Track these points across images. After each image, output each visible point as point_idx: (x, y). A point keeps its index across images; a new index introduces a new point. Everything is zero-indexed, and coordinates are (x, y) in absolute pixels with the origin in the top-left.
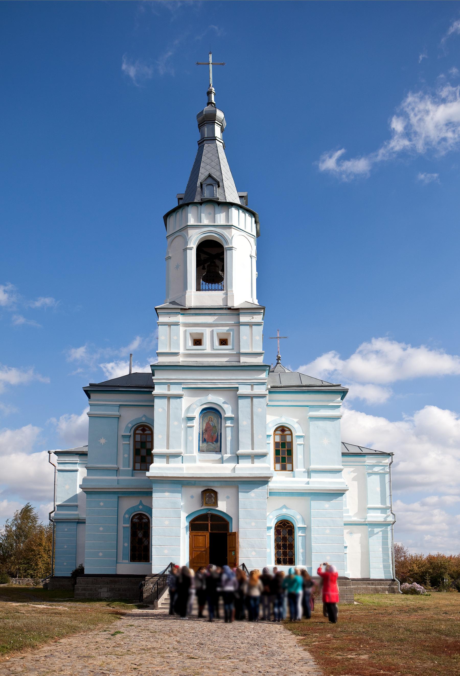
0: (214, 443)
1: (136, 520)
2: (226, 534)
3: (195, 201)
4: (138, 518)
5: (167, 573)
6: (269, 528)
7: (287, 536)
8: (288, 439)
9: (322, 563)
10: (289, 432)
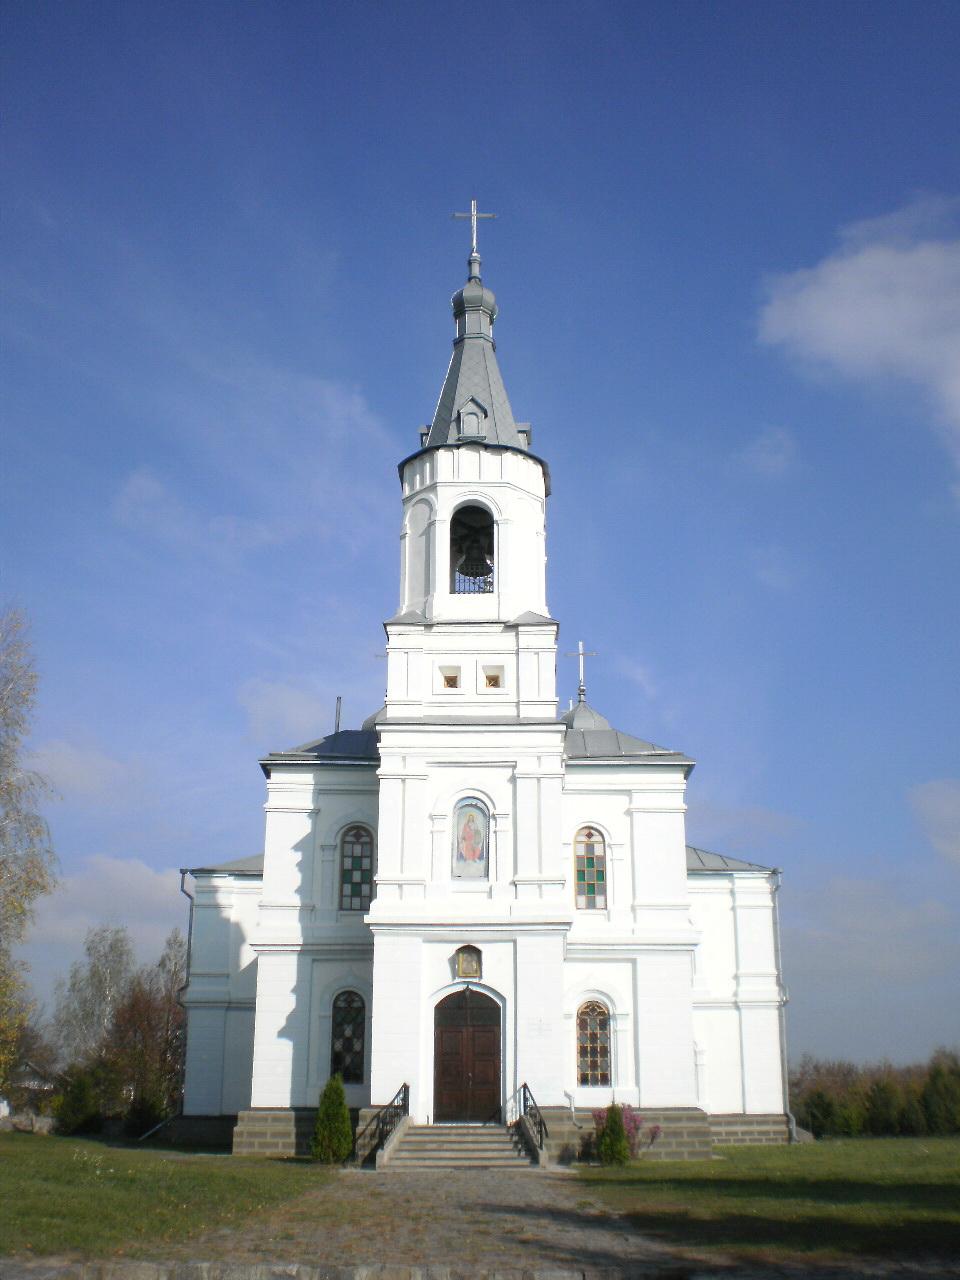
0: (478, 861)
1: (342, 1004)
3: (449, 442)
4: (345, 1000)
6: (568, 1016)
7: (598, 1031)
8: (598, 851)
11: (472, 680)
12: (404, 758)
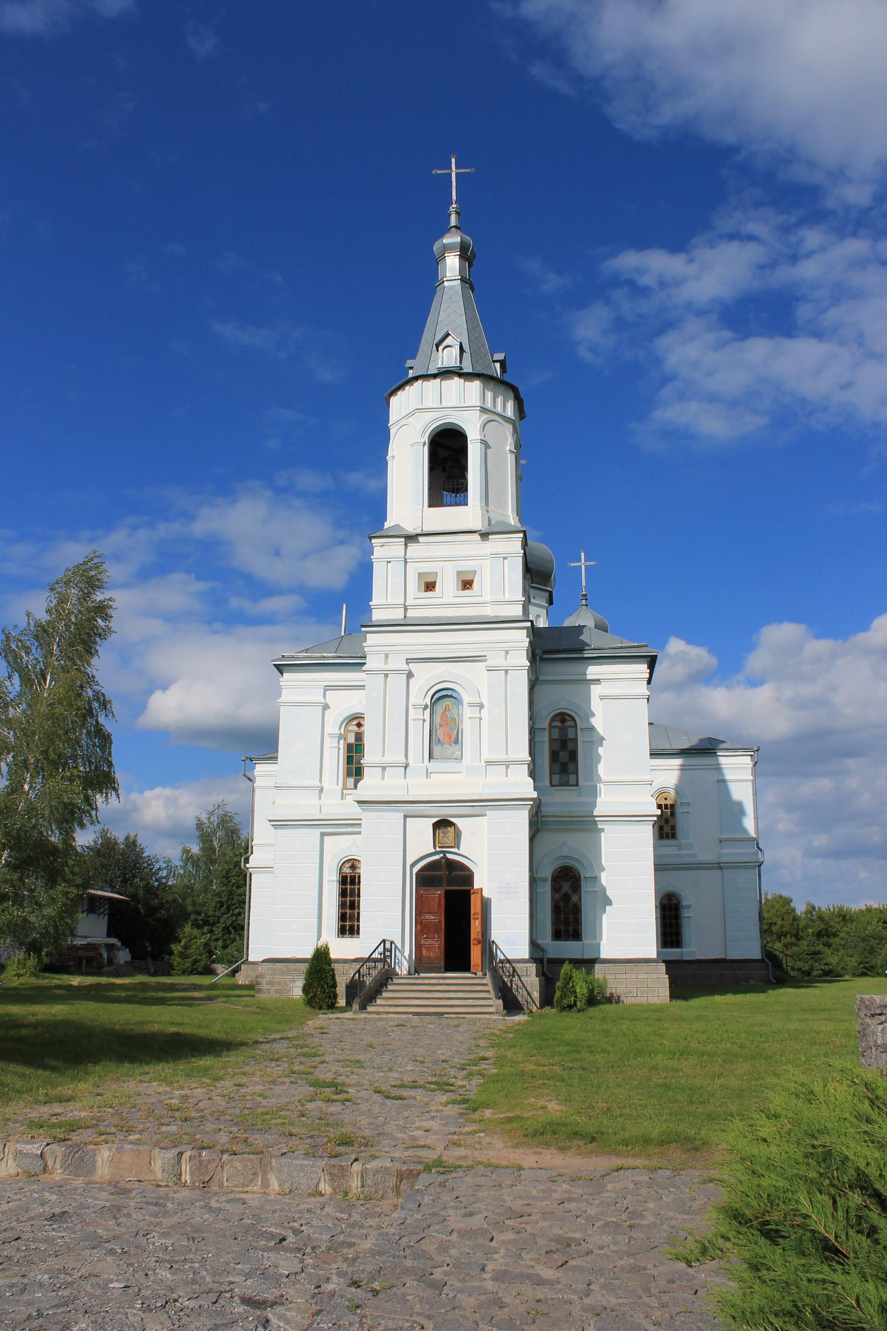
0: (453, 745)
2: (469, 891)
5: (376, 955)
8: (571, 734)
9: (391, 939)
10: (572, 723)
11: (448, 586)
12: (387, 656)
